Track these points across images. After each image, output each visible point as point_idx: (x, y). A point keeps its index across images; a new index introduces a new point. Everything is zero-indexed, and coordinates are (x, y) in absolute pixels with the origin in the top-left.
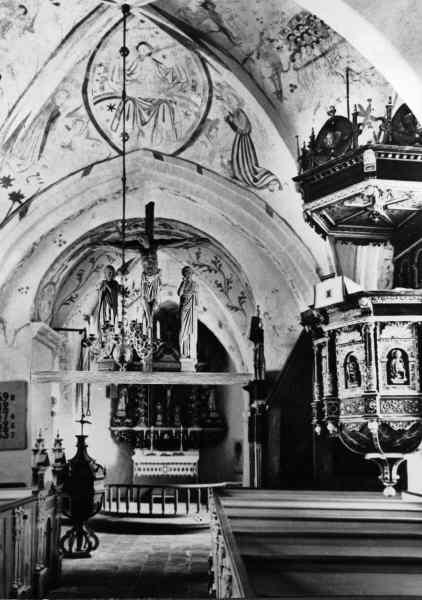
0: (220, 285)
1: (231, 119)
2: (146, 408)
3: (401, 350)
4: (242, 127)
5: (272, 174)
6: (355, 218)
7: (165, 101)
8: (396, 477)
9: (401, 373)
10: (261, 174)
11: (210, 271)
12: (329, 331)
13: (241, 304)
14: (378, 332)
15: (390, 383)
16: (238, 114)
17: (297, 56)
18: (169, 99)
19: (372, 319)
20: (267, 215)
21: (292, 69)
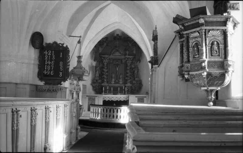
2: (107, 75)
3: (217, 42)
8: (213, 97)
9: (217, 52)
14: (207, 33)
15: (212, 55)
19: (204, 28)
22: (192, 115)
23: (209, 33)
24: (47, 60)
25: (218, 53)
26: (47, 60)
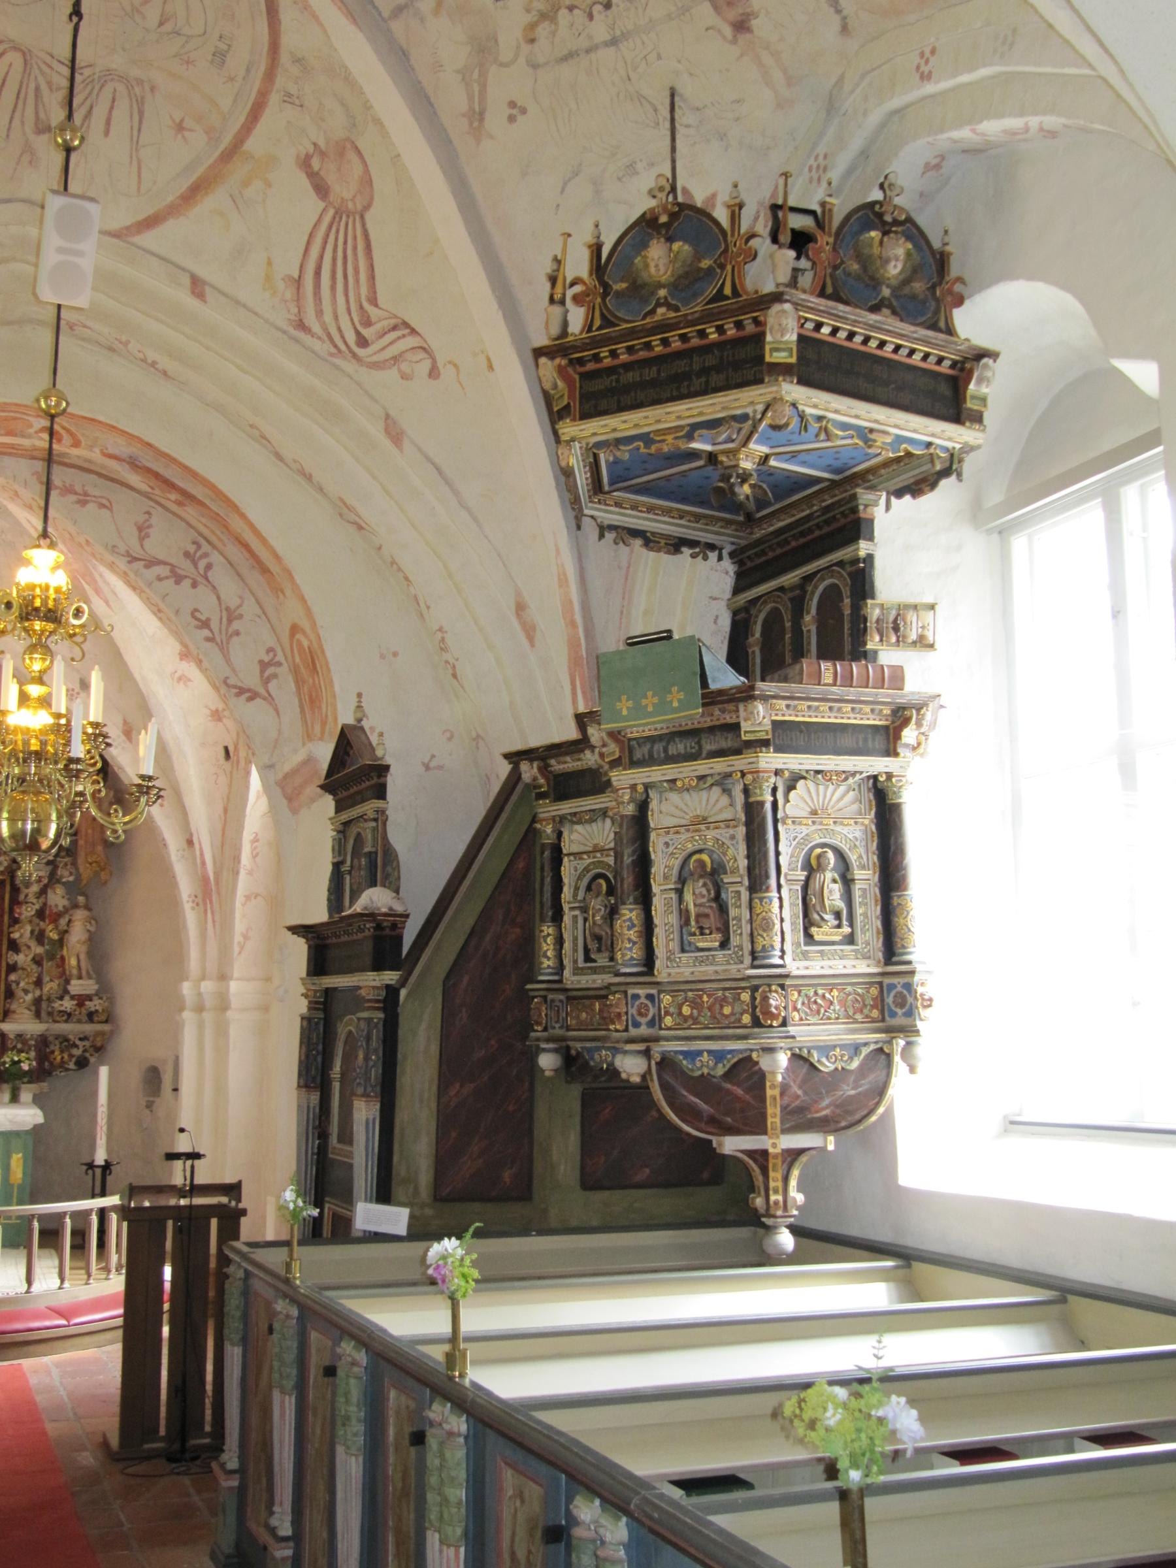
0: (205, 624)
1: (316, 164)
4: (344, 190)
5: (413, 331)
6: (668, 478)
7: (123, 79)
9: (838, 915)
10: (378, 327)
11: (179, 579)
12: (633, 787)
13: (266, 682)
15: (809, 937)
16: (341, 153)
17: (543, 30)
18: (135, 72)
19: (770, 760)
20: (387, 443)
21: (522, 60)
22: (14, 111)
23: (792, 794)
24: (80, 807)
25: (845, 922)
26: (80, 807)
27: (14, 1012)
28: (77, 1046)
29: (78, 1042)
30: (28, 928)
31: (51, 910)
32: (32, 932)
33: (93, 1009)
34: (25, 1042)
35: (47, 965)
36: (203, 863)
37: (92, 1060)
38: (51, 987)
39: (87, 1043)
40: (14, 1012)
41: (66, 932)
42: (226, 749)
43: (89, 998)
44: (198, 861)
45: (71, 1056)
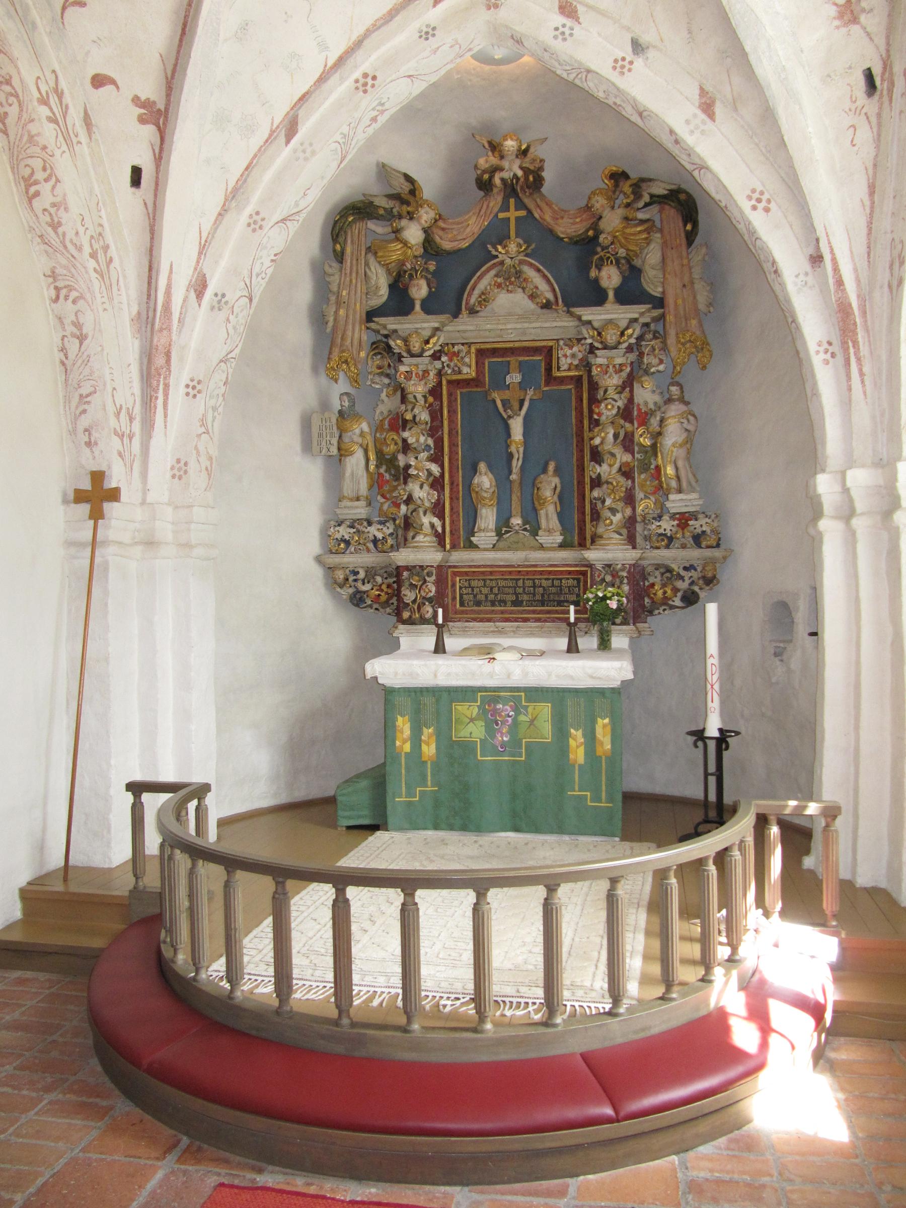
2: (437, 484)
27: (601, 537)
28: (682, 578)
29: (683, 573)
30: (611, 432)
31: (639, 410)
32: (616, 436)
33: (699, 531)
34: (615, 575)
35: (639, 478)
36: (840, 283)
37: (702, 594)
38: (644, 505)
39: (693, 573)
40: (601, 537)
41: (660, 434)
42: (869, 76)
43: (694, 516)
44: (831, 281)
45: (676, 590)
